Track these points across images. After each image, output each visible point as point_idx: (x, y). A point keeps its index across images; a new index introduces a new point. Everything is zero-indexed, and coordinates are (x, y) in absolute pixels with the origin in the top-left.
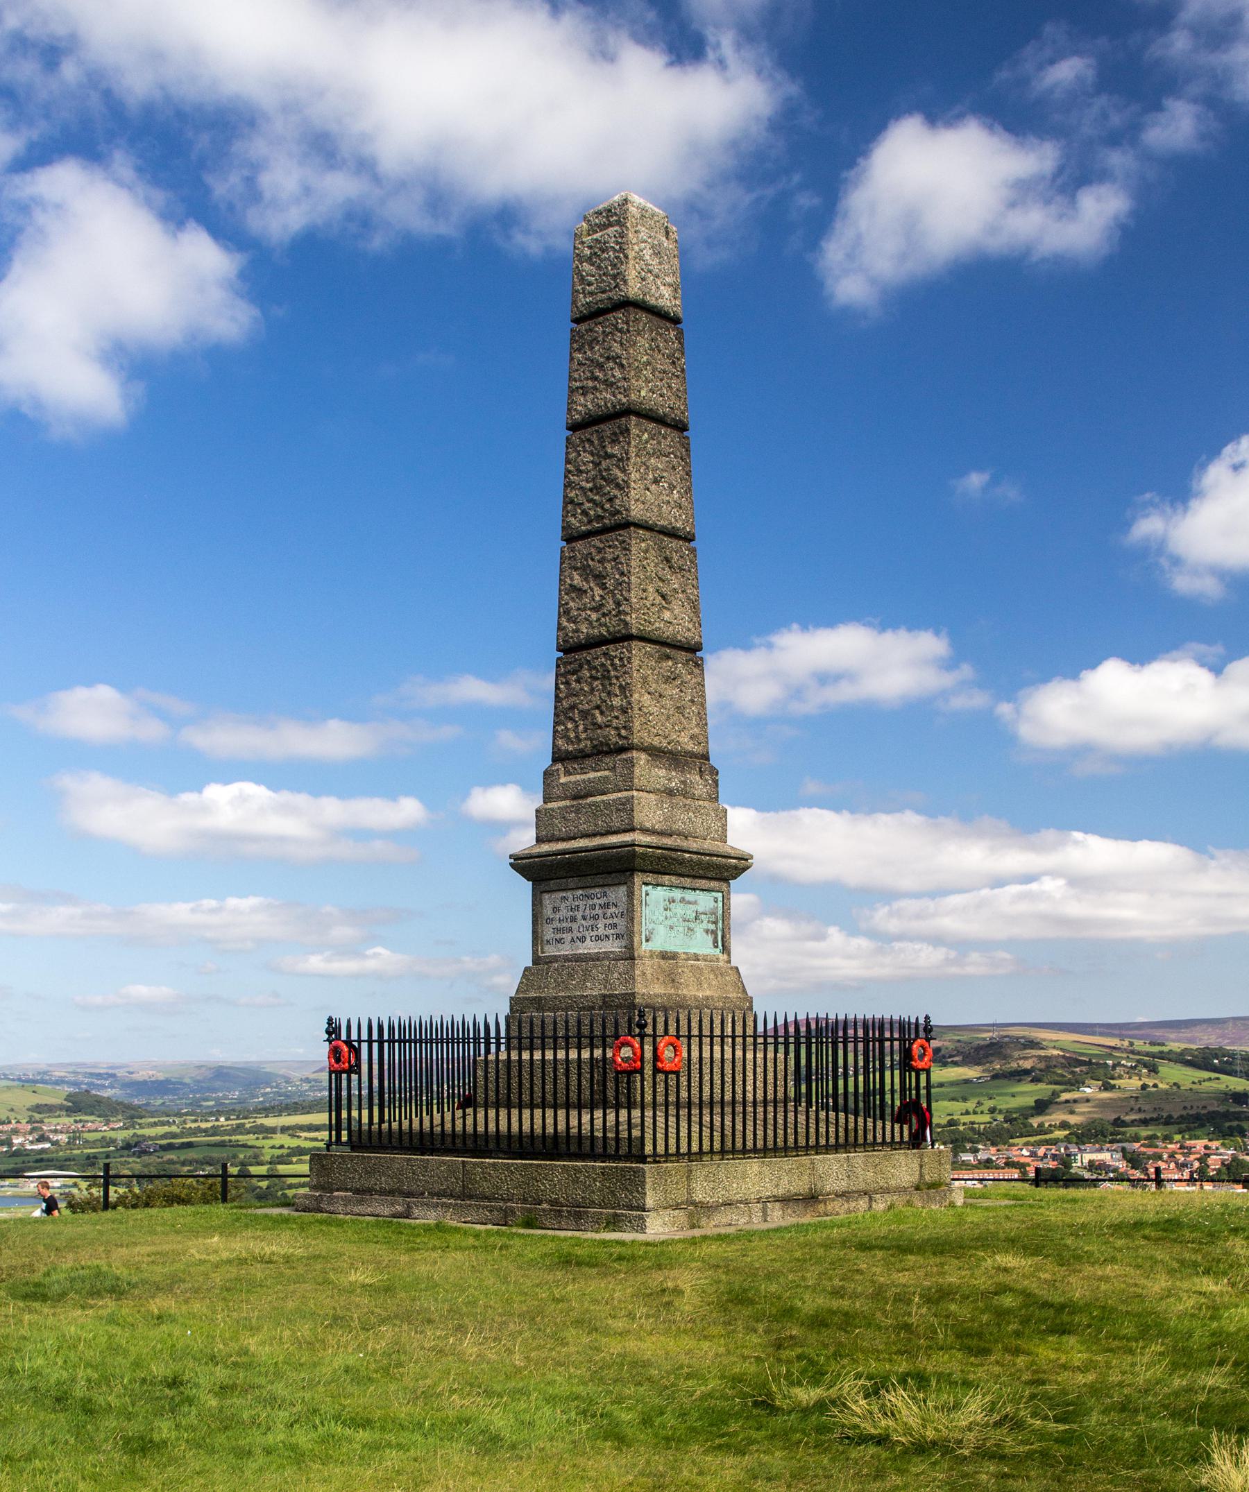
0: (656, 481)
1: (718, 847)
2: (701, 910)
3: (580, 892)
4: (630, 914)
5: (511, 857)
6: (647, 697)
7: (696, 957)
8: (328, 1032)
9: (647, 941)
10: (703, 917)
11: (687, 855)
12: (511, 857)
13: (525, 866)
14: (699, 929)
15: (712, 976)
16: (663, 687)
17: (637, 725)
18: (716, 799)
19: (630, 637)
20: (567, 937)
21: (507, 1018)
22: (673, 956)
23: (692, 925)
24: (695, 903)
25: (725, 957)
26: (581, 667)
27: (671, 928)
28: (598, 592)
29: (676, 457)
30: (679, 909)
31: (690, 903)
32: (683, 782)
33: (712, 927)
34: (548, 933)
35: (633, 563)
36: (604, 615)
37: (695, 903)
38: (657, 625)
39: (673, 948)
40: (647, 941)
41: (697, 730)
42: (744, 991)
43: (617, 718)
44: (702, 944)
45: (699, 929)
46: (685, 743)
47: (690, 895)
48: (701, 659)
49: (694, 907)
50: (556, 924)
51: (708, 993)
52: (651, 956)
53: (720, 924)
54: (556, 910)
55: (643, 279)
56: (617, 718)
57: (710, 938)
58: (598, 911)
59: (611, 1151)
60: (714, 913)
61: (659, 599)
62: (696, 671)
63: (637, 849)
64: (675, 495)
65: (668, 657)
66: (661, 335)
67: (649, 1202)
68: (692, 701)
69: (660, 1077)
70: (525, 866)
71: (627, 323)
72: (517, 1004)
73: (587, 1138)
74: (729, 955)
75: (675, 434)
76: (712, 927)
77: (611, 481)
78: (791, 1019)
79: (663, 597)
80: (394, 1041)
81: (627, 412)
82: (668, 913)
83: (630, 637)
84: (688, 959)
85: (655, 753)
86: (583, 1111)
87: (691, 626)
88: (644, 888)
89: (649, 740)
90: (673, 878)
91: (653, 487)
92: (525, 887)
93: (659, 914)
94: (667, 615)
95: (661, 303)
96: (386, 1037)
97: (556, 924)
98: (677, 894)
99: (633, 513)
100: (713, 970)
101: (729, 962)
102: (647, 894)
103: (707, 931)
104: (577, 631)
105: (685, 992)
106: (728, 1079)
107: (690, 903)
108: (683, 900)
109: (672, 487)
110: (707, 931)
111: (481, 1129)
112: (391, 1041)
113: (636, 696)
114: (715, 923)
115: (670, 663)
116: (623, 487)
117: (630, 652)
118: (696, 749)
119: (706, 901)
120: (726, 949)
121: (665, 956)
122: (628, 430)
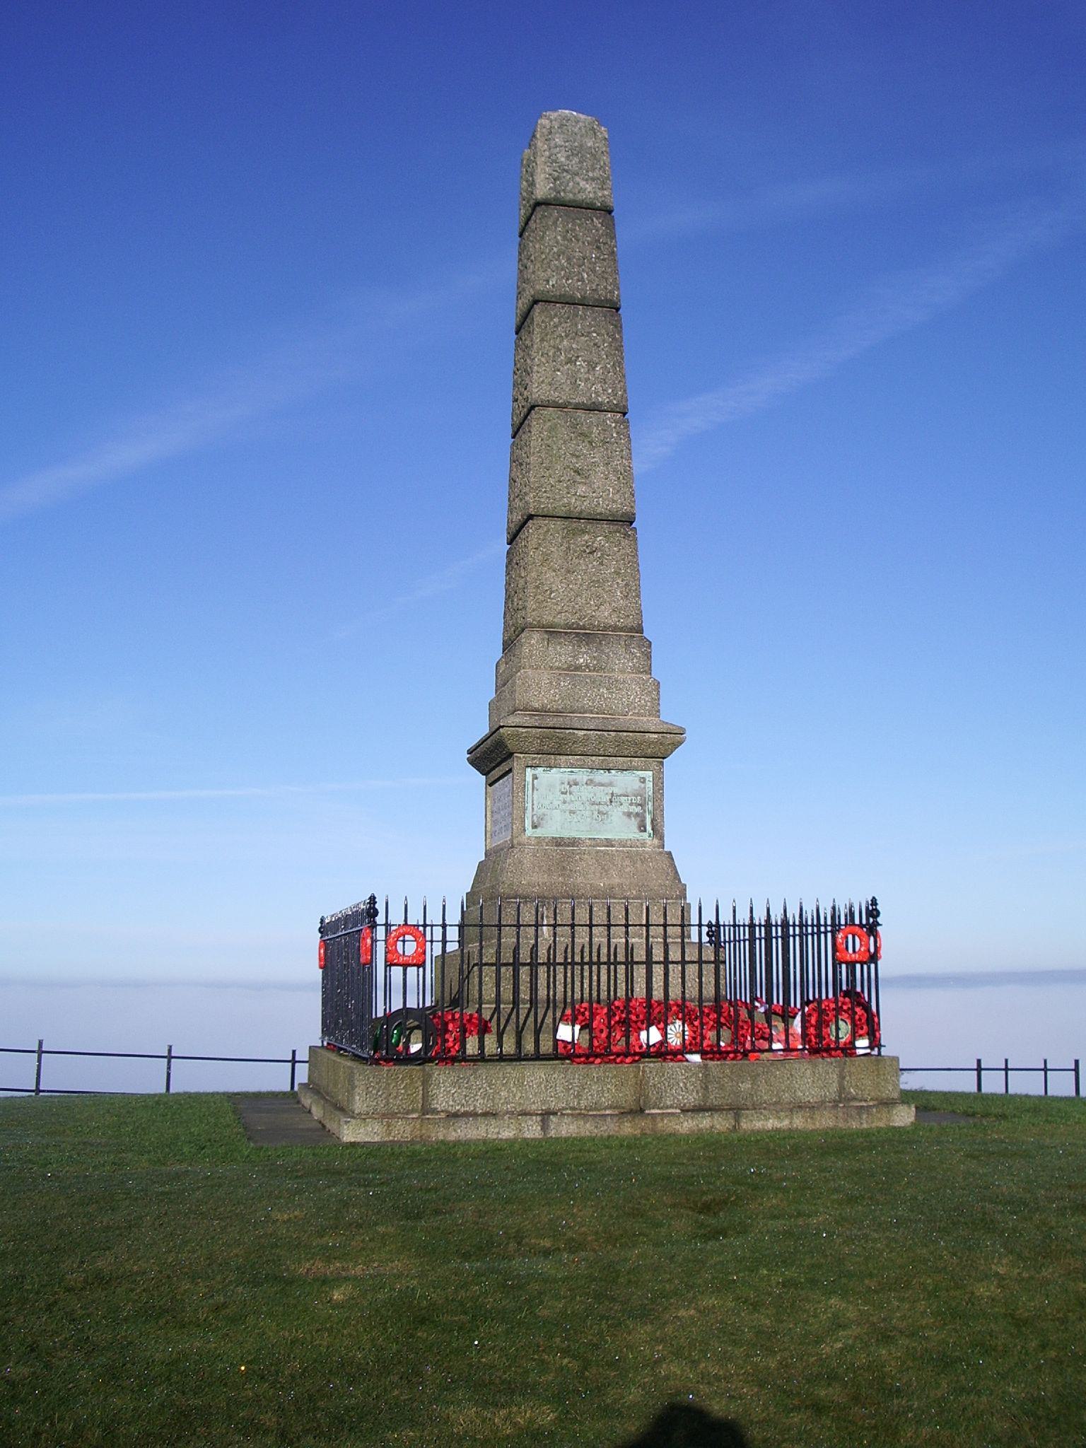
1: (649, 723)
2: (616, 790)
6: (551, 574)
9: (535, 827)
14: (616, 814)
18: (649, 672)
24: (611, 784)
25: (656, 841)
27: (572, 812)
30: (586, 792)
40: (535, 827)
45: (616, 814)
47: (601, 776)
57: (634, 822)
62: (625, 542)
69: (397, 972)
73: (659, 1003)
74: (661, 838)
78: (777, 917)
80: (608, 963)
82: (568, 797)
87: (617, 497)
94: (581, 490)
98: (582, 775)
102: (535, 777)
103: (629, 815)
105: (579, 880)
108: (590, 782)
110: (629, 815)
111: (658, 994)
112: (551, 964)
115: (587, 537)
119: (629, 781)
120: (658, 833)
121: (558, 842)
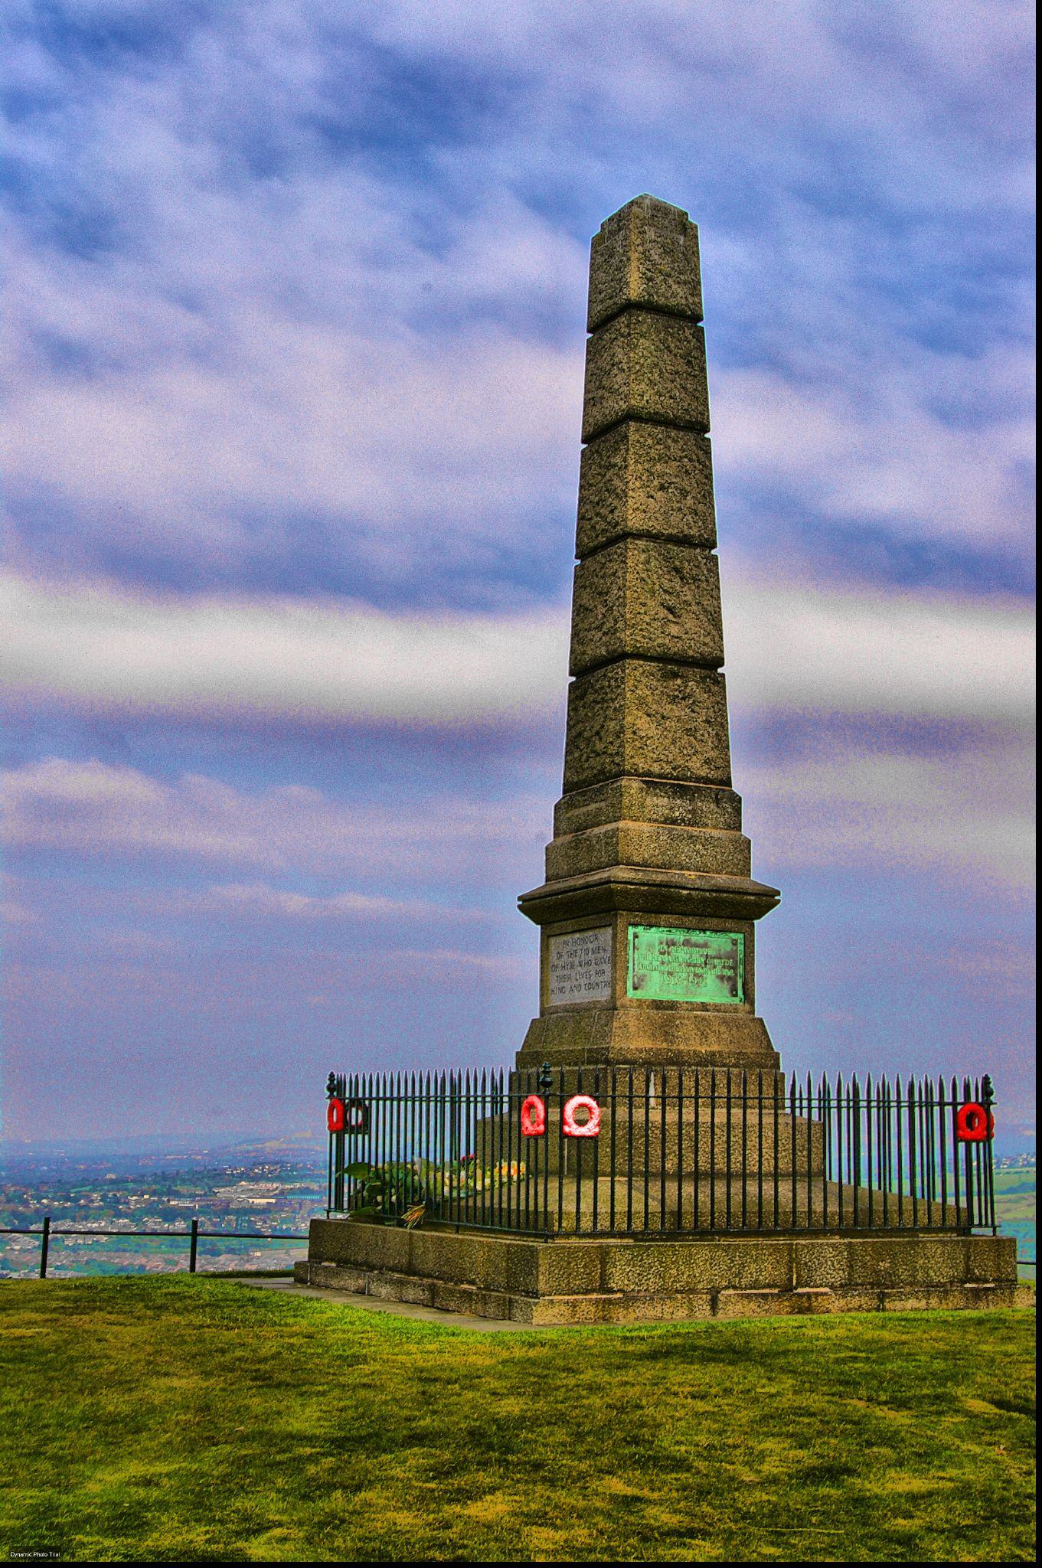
0: (662, 488)
2: (711, 952)
3: (578, 935)
4: (617, 958)
5: (519, 898)
7: (704, 1007)
8: (329, 1088)
9: (635, 988)
10: (716, 961)
11: (685, 892)
12: (519, 898)
13: (533, 906)
15: (723, 1029)
16: (667, 709)
17: (628, 751)
19: (625, 656)
20: (567, 985)
21: (511, 1075)
22: (672, 1006)
23: (699, 971)
24: (705, 945)
25: (747, 1007)
26: (586, 691)
27: (670, 974)
28: (601, 610)
29: (690, 460)
30: (682, 954)
31: (697, 945)
32: (693, 812)
33: (730, 973)
34: (553, 984)
35: (629, 577)
36: (605, 634)
37: (705, 945)
38: (660, 641)
39: (672, 997)
41: (713, 754)
42: (769, 1045)
43: (611, 743)
44: (712, 991)
46: (697, 767)
47: (698, 937)
48: (723, 675)
49: (705, 951)
50: (559, 972)
51: (715, 1048)
52: (640, 1006)
53: (741, 970)
54: (560, 955)
55: (650, 279)
56: (611, 743)
57: (726, 986)
58: (591, 956)
59: (586, 1224)
60: (731, 955)
61: (663, 613)
63: (613, 886)
64: (689, 501)
65: (675, 676)
66: (672, 335)
67: (542, 1286)
68: (708, 722)
70: (533, 906)
71: (628, 326)
72: (522, 1059)
74: (752, 1004)
75: (691, 436)
76: (730, 973)
77: (611, 491)
79: (671, 610)
81: (631, 416)
83: (625, 656)
84: (693, 1009)
85: (653, 783)
86: (701, 1183)
87: (707, 640)
88: (631, 930)
89: (642, 765)
90: (716, 921)
91: (659, 495)
92: (533, 931)
93: (655, 958)
95: (673, 302)
96: (936, 1109)
97: (559, 972)
98: (679, 936)
99: (630, 524)
100: (725, 1021)
101: (753, 1012)
102: (636, 936)
103: (721, 978)
104: (584, 653)
105: (682, 1047)
106: (409, 1141)
107: (697, 945)
108: (686, 943)
109: (684, 493)
113: (629, 719)
114: (734, 968)
115: (679, 681)
116: (622, 496)
117: (623, 671)
118: (712, 775)
119: (719, 942)
121: (658, 1005)
122: (626, 437)
